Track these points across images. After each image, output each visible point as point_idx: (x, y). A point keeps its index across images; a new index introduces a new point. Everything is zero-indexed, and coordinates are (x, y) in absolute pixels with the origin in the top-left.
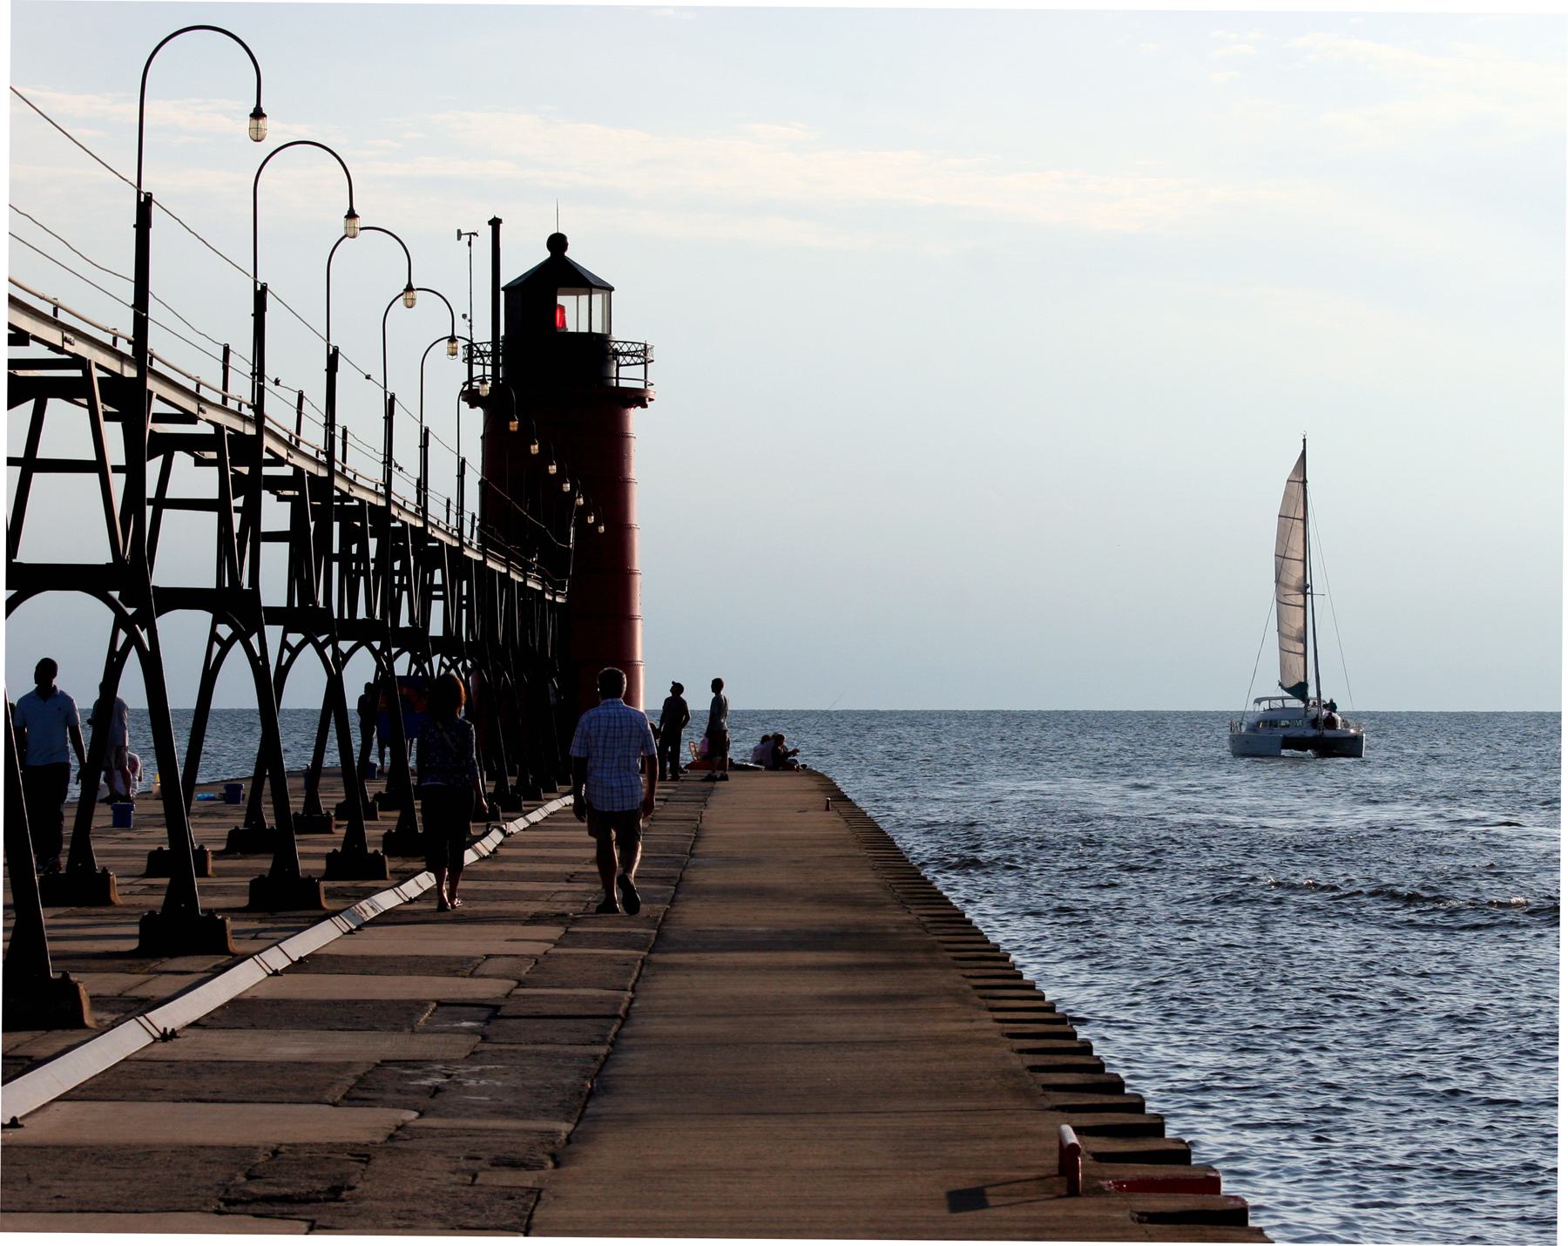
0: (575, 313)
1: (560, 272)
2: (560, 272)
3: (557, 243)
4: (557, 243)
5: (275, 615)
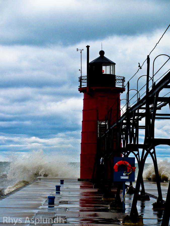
0: (106, 70)
1: (103, 60)
2: (103, 60)
3: (102, 53)
4: (102, 53)
5: (141, 146)
